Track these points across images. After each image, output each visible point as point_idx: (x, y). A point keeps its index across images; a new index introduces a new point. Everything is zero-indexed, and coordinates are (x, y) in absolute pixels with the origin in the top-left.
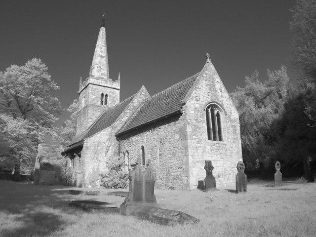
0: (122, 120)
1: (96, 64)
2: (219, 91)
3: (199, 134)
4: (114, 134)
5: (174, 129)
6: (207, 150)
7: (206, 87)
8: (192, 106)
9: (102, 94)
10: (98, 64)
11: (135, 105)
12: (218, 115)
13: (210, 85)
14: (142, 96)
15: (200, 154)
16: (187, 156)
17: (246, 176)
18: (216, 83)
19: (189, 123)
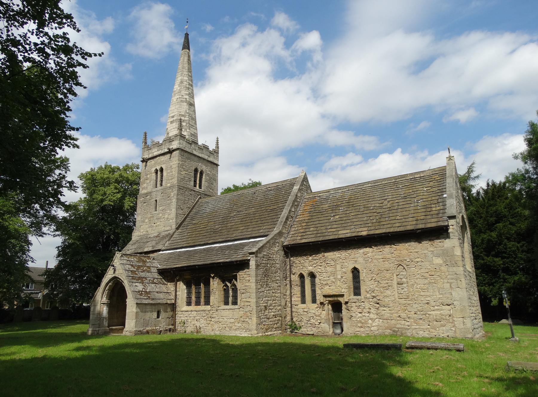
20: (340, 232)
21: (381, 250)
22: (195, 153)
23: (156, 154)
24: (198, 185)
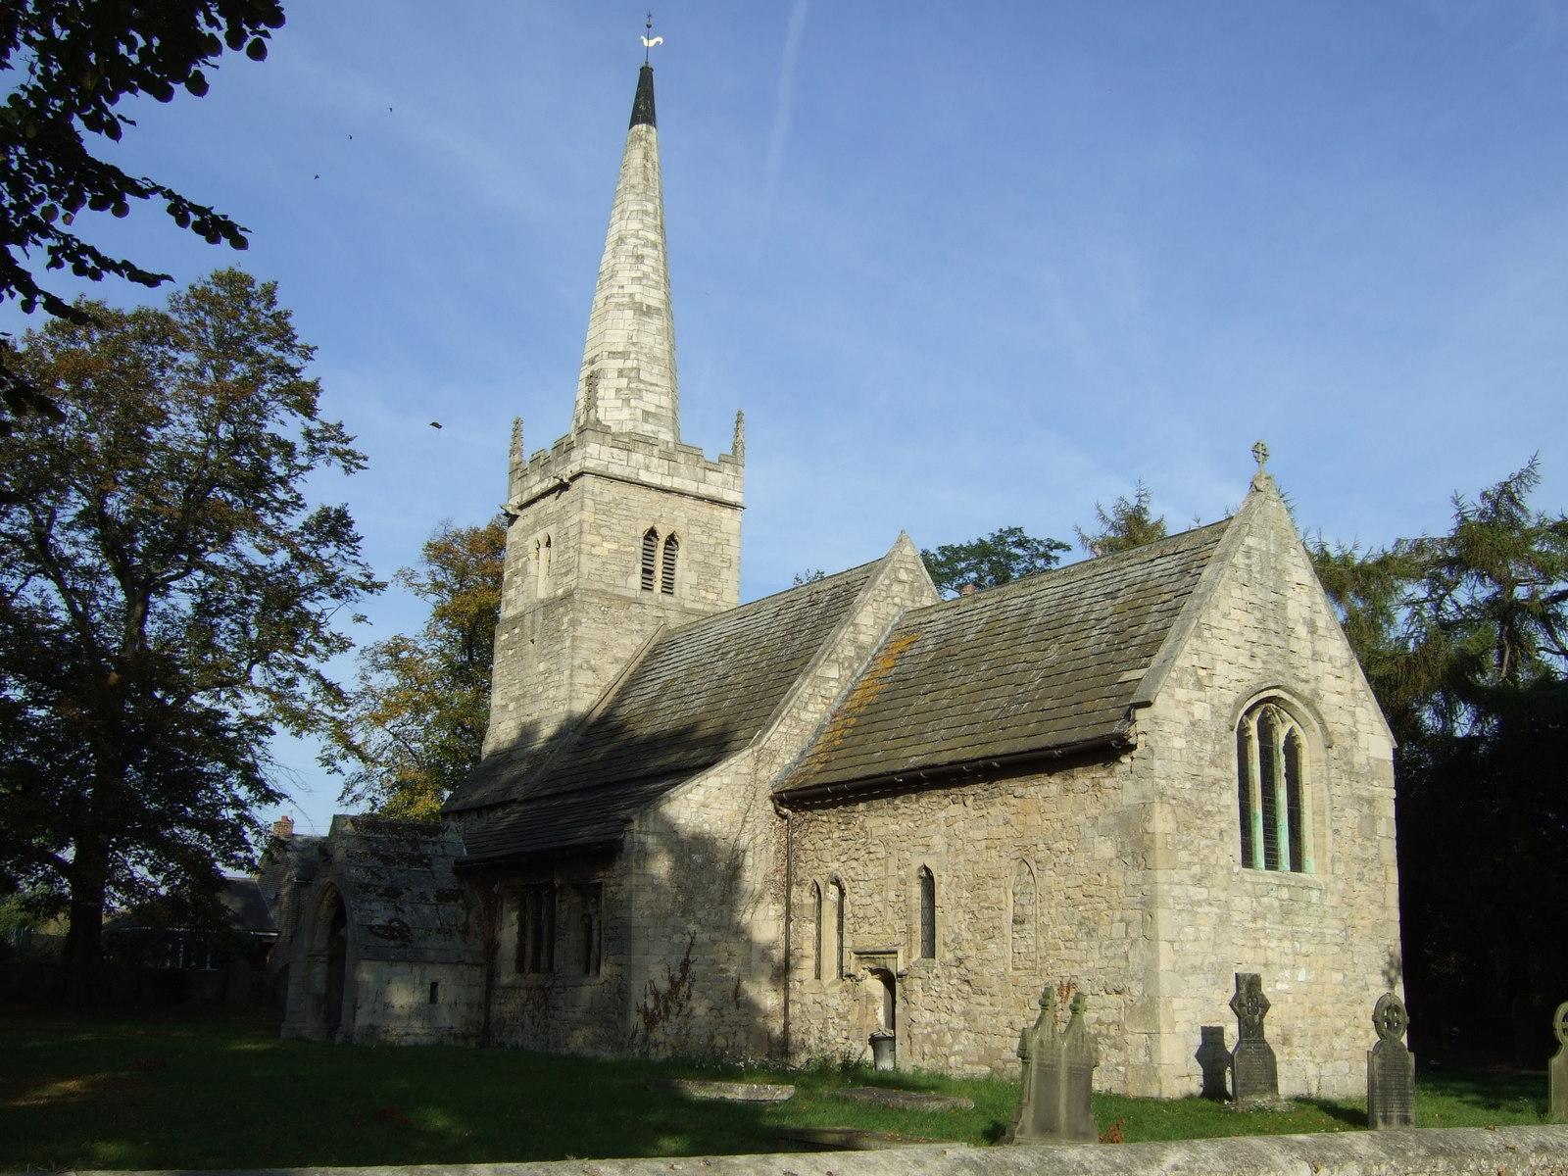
0: (804, 716)
1: (612, 355)
2: (1302, 631)
3: (1204, 842)
4: (766, 791)
5: (1093, 811)
6: (1237, 917)
7: (1246, 618)
8: (1179, 714)
9: (652, 534)
10: (624, 355)
11: (865, 639)
12: (1292, 748)
13: (1260, 608)
14: (896, 588)
15: (1206, 930)
16: (1151, 940)
17: (1412, 1057)
18: (1289, 593)
19: (1162, 794)
20: (906, 752)
21: (984, 812)
22: (645, 477)
23: (537, 489)
24: (658, 586)
